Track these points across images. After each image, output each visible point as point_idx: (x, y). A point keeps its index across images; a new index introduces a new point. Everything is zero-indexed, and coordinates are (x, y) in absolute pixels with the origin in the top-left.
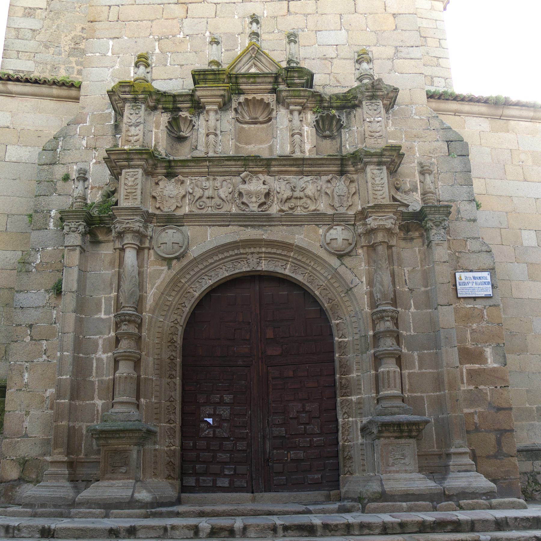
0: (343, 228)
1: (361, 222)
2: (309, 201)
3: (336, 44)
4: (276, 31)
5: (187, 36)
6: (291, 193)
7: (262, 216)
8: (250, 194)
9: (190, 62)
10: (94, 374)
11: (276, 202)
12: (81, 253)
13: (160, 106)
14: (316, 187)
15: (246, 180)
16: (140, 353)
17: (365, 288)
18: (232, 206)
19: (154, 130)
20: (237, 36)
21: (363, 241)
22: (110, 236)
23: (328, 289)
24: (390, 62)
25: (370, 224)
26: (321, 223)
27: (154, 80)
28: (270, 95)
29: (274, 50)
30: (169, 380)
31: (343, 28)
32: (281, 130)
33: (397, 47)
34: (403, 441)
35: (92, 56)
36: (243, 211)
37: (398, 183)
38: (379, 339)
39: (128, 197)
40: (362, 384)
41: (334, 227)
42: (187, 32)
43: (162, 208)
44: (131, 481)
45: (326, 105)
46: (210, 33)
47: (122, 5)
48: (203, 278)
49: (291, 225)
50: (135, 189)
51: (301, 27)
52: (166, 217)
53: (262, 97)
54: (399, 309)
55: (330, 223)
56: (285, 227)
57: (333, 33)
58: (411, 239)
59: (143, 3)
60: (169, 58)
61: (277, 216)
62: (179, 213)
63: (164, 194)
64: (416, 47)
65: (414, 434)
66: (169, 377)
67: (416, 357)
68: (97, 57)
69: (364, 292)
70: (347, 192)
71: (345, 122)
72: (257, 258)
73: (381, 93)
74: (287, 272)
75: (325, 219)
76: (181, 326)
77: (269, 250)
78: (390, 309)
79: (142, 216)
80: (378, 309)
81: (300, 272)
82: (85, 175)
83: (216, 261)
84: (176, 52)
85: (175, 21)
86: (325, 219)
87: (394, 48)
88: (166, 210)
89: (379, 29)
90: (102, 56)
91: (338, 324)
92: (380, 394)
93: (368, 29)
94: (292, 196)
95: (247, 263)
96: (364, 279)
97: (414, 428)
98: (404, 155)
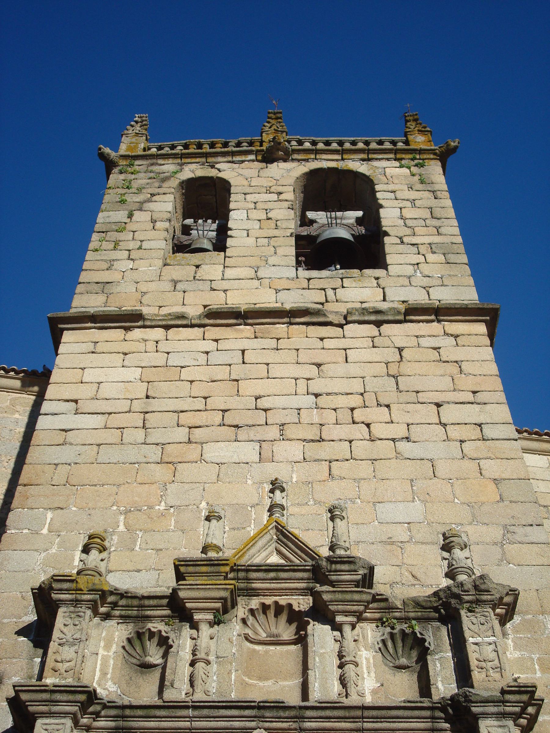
3: (407, 521)
13: (117, 613)
19: (101, 652)
28: (303, 599)
31: (416, 498)
32: (322, 655)
33: (506, 525)
42: (171, 502)
47: (76, 463)
57: (401, 506)
60: (139, 539)
64: (537, 525)
73: (489, 597)
85: (154, 486)
89: (473, 500)
93: (456, 500)
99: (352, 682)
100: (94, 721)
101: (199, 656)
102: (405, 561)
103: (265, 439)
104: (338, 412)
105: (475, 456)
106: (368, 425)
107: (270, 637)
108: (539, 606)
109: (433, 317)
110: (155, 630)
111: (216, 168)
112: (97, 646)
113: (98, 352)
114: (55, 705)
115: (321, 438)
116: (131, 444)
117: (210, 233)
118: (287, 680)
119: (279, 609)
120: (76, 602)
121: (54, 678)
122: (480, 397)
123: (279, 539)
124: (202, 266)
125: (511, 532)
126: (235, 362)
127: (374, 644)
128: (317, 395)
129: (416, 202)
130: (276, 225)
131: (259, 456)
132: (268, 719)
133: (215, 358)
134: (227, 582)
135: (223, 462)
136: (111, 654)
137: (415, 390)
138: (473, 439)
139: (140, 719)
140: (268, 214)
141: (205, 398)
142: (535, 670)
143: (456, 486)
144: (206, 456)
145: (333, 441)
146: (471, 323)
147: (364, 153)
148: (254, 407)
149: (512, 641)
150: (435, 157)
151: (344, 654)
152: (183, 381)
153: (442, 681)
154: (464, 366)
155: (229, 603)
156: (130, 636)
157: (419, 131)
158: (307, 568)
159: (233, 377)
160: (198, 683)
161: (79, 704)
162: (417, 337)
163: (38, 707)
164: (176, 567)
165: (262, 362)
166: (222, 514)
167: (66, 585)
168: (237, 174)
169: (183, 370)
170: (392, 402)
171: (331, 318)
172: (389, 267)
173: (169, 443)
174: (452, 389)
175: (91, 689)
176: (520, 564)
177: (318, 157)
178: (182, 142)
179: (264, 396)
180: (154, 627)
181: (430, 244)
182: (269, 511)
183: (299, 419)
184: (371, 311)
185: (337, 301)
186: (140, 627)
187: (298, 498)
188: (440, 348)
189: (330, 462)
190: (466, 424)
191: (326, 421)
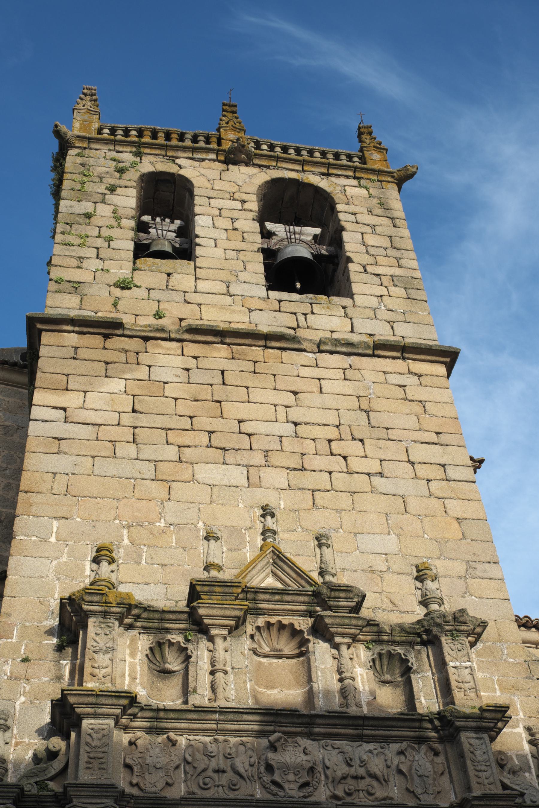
2: (375, 783)
3: (384, 553)
4: (300, 530)
5: (171, 524)
8: (286, 768)
9: (177, 562)
11: (323, 783)
13: (139, 624)
14: (383, 761)
15: (276, 744)
18: (256, 786)
19: (128, 659)
20: (243, 531)
24: (461, 582)
27: (122, 583)
28: (303, 620)
29: (299, 555)
31: (391, 531)
32: (323, 670)
33: (468, 561)
35: (26, 540)
37: (503, 758)
39: (90, 766)
42: (171, 520)
43: (142, 785)
45: (386, 638)
46: (205, 524)
47: (73, 474)
50: (103, 752)
51: (333, 526)
52: (152, 801)
53: (291, 621)
57: (378, 537)
59: (104, 475)
60: (144, 554)
63: (147, 762)
64: (494, 563)
68: (34, 542)
70: (432, 770)
71: (414, 664)
73: (465, 628)
82: (6, 720)
84: (154, 546)
85: (152, 503)
87: (464, 563)
89: (440, 536)
90: (41, 541)
93: (426, 536)
94: (348, 774)
98: (510, 718)
99: (352, 695)
100: (131, 721)
101: (218, 667)
102: (384, 589)
103: (252, 464)
104: (317, 442)
105: (440, 495)
106: (345, 458)
107: (274, 651)
108: (497, 635)
109: (398, 354)
110: (174, 641)
111: (177, 164)
112: (124, 654)
113: (80, 358)
114: (100, 708)
115: (303, 467)
116: (125, 458)
117: (169, 233)
118: (290, 689)
119: (282, 627)
120: (105, 614)
121: (93, 683)
122: (444, 439)
123: (274, 563)
124: (174, 274)
125: (473, 568)
126: (216, 382)
127: (366, 662)
128: (296, 424)
129: (376, 228)
130: (243, 238)
131: (247, 480)
132: (283, 725)
133: (196, 376)
134: (237, 602)
135: (214, 484)
136: (137, 660)
137: (385, 426)
138: (438, 478)
139: (172, 721)
140: (234, 223)
141: (191, 417)
142: (495, 689)
143: (424, 522)
144: (198, 476)
145: (314, 471)
146: (433, 364)
147: (325, 167)
148: (238, 431)
149: (476, 664)
150: (393, 180)
151: (343, 670)
152: (167, 397)
153: (424, 696)
154: (428, 406)
155: (241, 621)
156: (152, 646)
157: (374, 147)
158: (308, 593)
159: (216, 398)
160: (220, 691)
161: (122, 707)
162: (384, 372)
163: (84, 709)
164: (192, 587)
165: (241, 385)
166: (219, 535)
167: (96, 598)
168: (198, 174)
169: (166, 385)
170: (365, 437)
171: (305, 345)
172: (355, 296)
173: (161, 461)
174: (418, 429)
175: (134, 695)
176: (481, 596)
177: (279, 165)
178: (136, 126)
179: (247, 421)
180: (173, 639)
181: (392, 276)
182: (262, 534)
183: (281, 446)
184: (343, 342)
185: (308, 327)
186: (160, 637)
187: (287, 524)
188: (405, 386)
189: (313, 491)
190: (431, 464)
191: (307, 451)
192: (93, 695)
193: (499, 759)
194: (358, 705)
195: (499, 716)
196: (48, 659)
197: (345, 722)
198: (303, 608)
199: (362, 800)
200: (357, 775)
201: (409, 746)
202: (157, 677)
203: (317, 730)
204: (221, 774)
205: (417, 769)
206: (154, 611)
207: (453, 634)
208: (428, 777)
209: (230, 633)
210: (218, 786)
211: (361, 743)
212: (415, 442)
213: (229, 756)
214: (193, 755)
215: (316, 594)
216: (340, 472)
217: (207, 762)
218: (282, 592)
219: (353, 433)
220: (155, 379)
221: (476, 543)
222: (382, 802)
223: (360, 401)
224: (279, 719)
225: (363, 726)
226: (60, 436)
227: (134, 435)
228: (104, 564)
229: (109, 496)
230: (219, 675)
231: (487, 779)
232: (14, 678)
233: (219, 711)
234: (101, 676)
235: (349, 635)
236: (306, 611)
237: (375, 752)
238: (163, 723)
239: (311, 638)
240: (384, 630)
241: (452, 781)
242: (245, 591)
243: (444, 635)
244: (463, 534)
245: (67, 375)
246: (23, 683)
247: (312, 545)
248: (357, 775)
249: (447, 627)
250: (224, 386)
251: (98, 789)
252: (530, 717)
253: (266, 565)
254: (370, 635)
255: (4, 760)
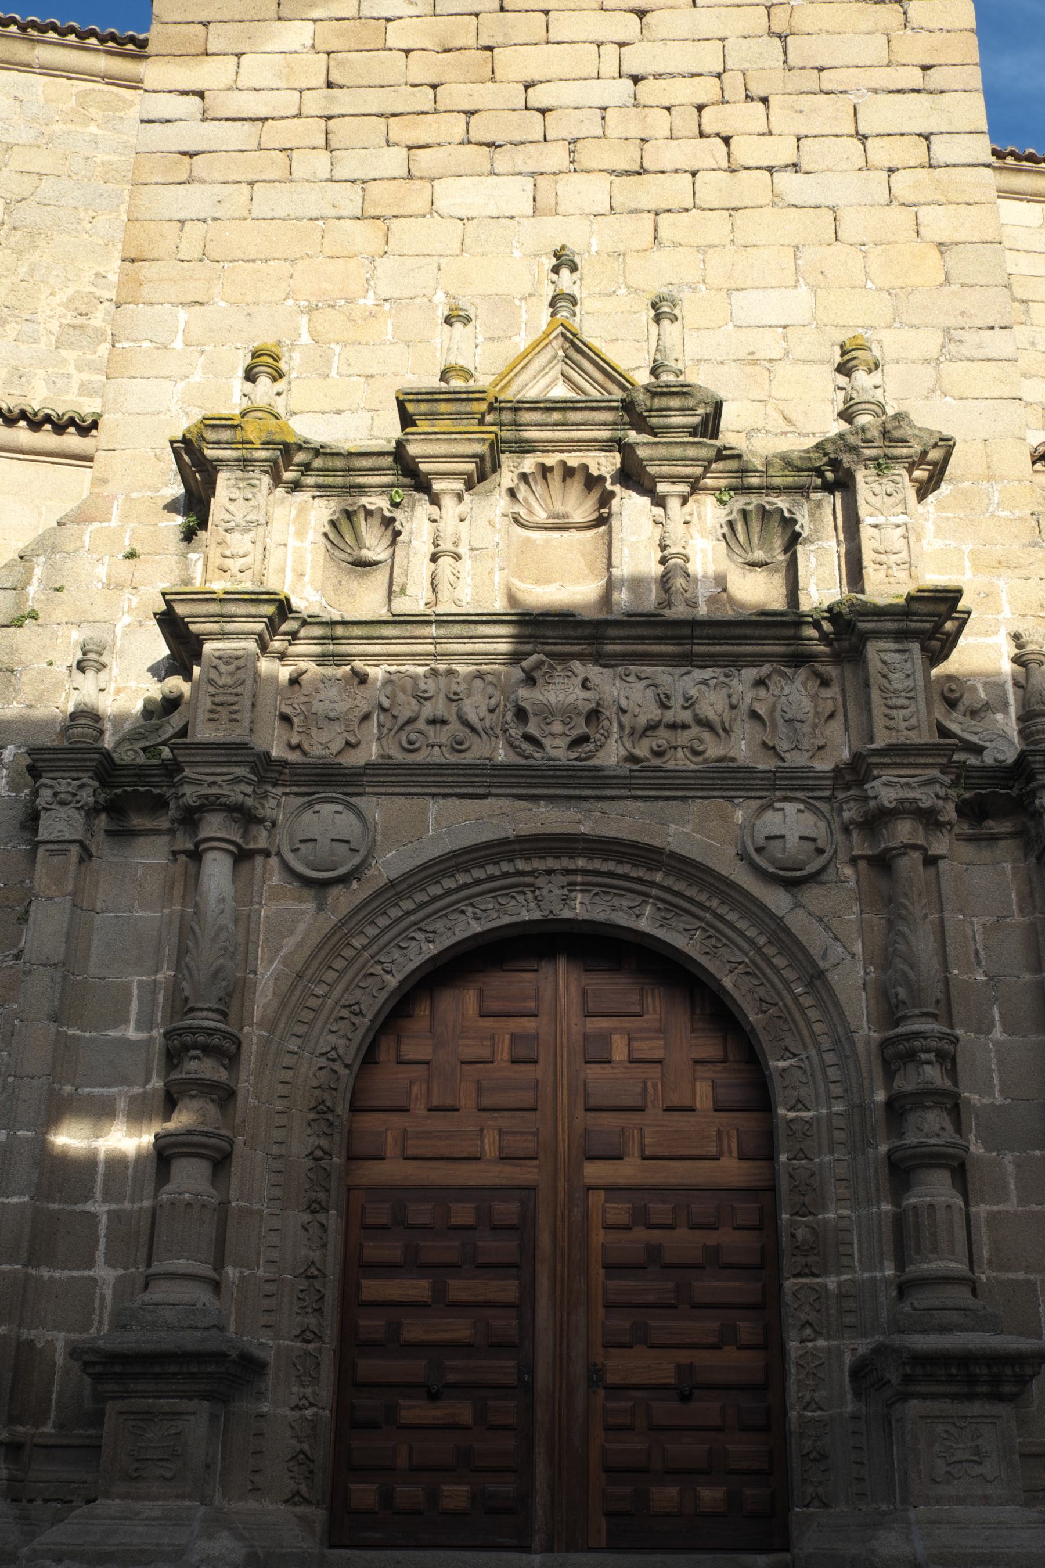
0: (802, 806)
1: (851, 792)
2: (707, 736)
4: (623, 291)
6: (659, 712)
7: (579, 773)
8: (547, 713)
10: (98, 1195)
12: (81, 861)
13: (310, 481)
14: (726, 697)
15: (535, 674)
16: (231, 1136)
17: (862, 973)
18: (497, 744)
19: (292, 542)
20: (517, 302)
21: (861, 847)
22: (163, 819)
23: (757, 972)
24: (930, 369)
25: (876, 798)
26: (739, 793)
28: (606, 457)
29: (617, 340)
30: (307, 1217)
33: (949, 328)
34: (977, 1408)
35: (132, 349)
36: (527, 758)
37: (954, 687)
38: (902, 1115)
39: (215, 716)
40: (855, 1241)
41: (778, 805)
43: (306, 747)
44: (187, 1503)
45: (755, 481)
46: (447, 294)
47: (215, 219)
48: (413, 938)
49: (657, 798)
50: (237, 695)
52: (318, 771)
53: (584, 461)
54: (959, 1032)
55: (765, 793)
56: (640, 804)
58: (992, 839)
60: (336, 358)
61: (621, 773)
62: (355, 759)
63: (314, 710)
64: (1001, 328)
65: (1007, 1389)
66: (309, 1207)
67: (1011, 1168)
69: (860, 983)
70: (812, 711)
71: (806, 528)
72: (563, 887)
74: (644, 925)
75: (752, 782)
76: (347, 1066)
77: (597, 865)
78: (932, 1031)
79: (252, 768)
80: (900, 1030)
81: (681, 926)
83: (449, 892)
85: (353, 263)
86: (752, 782)
87: (940, 333)
88: (317, 751)
90: (158, 348)
91: (784, 1070)
92: (907, 1270)
93: (869, 285)
94: (660, 721)
95: (536, 898)
96: (858, 948)
97: (1009, 1371)
98: (969, 613)
100: (290, 644)
102: (774, 394)
103: (543, 170)
105: (911, 198)
106: (727, 140)
115: (642, 167)
116: (308, 181)
119: (568, 472)
120: (245, 463)
123: (567, 357)
128: (636, 79)
135: (470, 216)
137: (817, 65)
138: (912, 164)
141: (434, 87)
145: (663, 172)
148: (522, 105)
151: (667, 543)
152: (390, 49)
153: (816, 584)
155: (488, 465)
156: (334, 517)
159: (485, 41)
160: (443, 587)
167: (226, 435)
169: (390, 25)
173: (375, 180)
174: (885, 62)
175: (282, 597)
176: (964, 396)
179: (541, 82)
183: (604, 128)
190: (902, 135)
192: (214, 600)
193: (946, 689)
194: (690, 603)
195: (943, 608)
196: (167, 552)
197: (659, 632)
198: (606, 434)
199: (681, 762)
200: (675, 722)
201: (775, 670)
202: (349, 574)
203: (610, 648)
204: (438, 726)
205: (785, 709)
206: (333, 454)
207: (879, 465)
208: (802, 722)
209: (469, 487)
210: (433, 746)
211: (689, 668)
212: (875, 91)
213: (454, 697)
214: (392, 697)
215: (628, 406)
216: (714, 170)
217: (416, 708)
218: (564, 405)
219: (748, 87)
220: (369, 15)
221: (970, 290)
222: (718, 764)
223: (772, 14)
224: (542, 631)
225: (692, 638)
226: (192, 148)
227: (327, 133)
228: (263, 381)
229: (277, 256)
230: (445, 561)
231: (905, 721)
232: (114, 585)
233: (436, 621)
234: (235, 571)
235: (683, 477)
236: (610, 440)
237: (712, 682)
238: (344, 647)
239: (617, 488)
240: (751, 467)
241: (847, 729)
242: (496, 409)
243: (863, 468)
244: (946, 273)
245: (206, 24)
246: (127, 593)
247: (644, 319)
248: (675, 722)
249: (868, 452)
250: (502, 14)
251: (223, 751)
252: (1023, 616)
253: (551, 362)
254: (726, 478)
255: (97, 715)
